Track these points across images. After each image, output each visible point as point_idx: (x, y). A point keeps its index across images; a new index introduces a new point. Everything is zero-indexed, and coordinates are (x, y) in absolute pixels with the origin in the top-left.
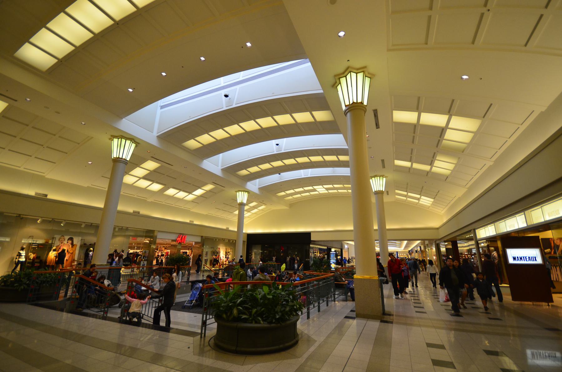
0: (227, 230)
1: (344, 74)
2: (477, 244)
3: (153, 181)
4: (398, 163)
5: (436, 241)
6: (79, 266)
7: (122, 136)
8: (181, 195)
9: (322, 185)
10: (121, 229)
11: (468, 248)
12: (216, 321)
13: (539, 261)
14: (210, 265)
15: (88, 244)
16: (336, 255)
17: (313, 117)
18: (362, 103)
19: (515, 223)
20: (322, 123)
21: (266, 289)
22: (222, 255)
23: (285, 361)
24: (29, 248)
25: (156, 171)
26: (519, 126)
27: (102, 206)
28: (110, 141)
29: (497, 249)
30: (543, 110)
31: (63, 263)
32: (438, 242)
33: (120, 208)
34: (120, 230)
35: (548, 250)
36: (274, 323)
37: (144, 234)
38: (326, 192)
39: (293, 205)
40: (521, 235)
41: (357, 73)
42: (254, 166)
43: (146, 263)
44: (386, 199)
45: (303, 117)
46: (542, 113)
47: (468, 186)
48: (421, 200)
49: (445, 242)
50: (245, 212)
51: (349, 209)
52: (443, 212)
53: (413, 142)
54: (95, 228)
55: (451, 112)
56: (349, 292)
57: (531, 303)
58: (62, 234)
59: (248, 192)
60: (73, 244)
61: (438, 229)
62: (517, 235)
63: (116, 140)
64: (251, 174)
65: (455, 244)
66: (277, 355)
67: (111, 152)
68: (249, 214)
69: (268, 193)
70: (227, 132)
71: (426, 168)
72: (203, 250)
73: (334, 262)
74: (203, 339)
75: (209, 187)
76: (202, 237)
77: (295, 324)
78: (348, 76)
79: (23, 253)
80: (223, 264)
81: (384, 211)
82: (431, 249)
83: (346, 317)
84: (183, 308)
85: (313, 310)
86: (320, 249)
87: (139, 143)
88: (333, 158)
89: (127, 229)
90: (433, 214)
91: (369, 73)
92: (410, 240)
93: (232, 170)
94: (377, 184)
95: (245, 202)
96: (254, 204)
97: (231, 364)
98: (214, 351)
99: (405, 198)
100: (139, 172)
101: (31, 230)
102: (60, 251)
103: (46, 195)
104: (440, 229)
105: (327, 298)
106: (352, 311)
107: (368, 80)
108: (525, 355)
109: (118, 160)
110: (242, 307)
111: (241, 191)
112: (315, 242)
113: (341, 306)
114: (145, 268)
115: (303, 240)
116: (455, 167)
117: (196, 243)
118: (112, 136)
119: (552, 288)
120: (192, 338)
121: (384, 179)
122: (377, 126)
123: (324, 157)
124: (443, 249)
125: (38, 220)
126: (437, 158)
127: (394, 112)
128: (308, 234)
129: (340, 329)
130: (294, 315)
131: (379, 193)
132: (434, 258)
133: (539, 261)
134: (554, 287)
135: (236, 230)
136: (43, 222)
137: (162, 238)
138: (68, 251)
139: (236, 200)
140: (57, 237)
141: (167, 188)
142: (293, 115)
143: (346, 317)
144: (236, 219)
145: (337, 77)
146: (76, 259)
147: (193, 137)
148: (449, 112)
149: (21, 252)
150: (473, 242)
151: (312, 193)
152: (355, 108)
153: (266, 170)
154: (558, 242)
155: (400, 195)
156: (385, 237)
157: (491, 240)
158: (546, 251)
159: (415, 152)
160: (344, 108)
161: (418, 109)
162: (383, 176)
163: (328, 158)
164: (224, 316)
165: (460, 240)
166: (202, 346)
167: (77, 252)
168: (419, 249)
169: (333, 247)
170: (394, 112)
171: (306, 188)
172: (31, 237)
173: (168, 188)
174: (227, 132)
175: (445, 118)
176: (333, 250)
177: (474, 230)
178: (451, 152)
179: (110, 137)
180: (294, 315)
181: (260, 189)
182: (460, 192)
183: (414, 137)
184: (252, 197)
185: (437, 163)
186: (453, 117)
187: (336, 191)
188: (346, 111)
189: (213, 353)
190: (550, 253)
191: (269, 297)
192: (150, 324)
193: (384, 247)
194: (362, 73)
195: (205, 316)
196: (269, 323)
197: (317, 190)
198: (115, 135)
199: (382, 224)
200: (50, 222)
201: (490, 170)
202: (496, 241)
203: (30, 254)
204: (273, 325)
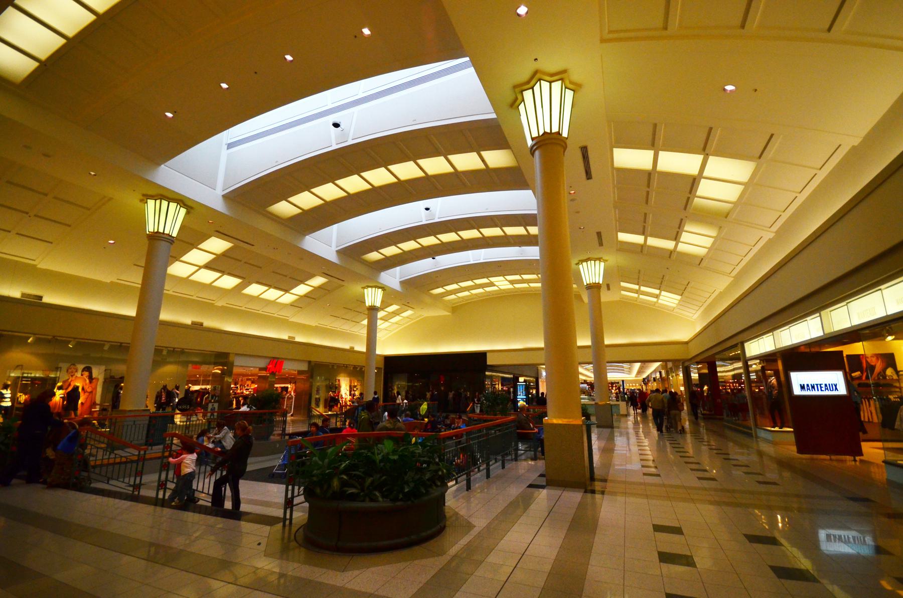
0: (351, 350)
1: (528, 84)
2: (746, 367)
3: (223, 272)
4: (623, 237)
5: (684, 361)
6: (104, 413)
7: (161, 195)
8: (272, 294)
9: (504, 276)
10: (173, 352)
11: (732, 373)
12: (306, 500)
13: (842, 390)
14: (325, 407)
15: (117, 377)
16: (527, 388)
17: (483, 161)
18: (558, 133)
19: (804, 331)
20: (498, 171)
21: (388, 446)
22: (344, 391)
23: (416, 562)
24: (17, 385)
25: (225, 255)
26: (815, 171)
27: (131, 312)
28: (141, 204)
29: (777, 374)
30: (856, 144)
31: (76, 409)
32: (686, 364)
33: (164, 316)
34: (161, 356)
35: (857, 374)
36: (401, 500)
37: (213, 360)
38: (511, 286)
39: (456, 308)
40: (813, 350)
41: (550, 82)
42: (390, 245)
43: (216, 405)
44: (606, 297)
45: (466, 161)
46: (854, 148)
47: (734, 274)
48: (661, 297)
49: (698, 363)
50: (379, 322)
51: (536, 313)
52: (696, 316)
53: (647, 203)
54: (122, 348)
55: (707, 151)
56: (537, 446)
57: (828, 457)
58: (73, 361)
59: (383, 288)
60: (91, 378)
61: (687, 343)
62: (808, 350)
63: (151, 202)
64: (387, 258)
65: (712, 367)
66: (405, 552)
67: (143, 223)
68: (387, 324)
69: (417, 289)
70: (341, 189)
71: (669, 244)
72: (311, 383)
73: (522, 399)
74: (287, 528)
75: (318, 281)
76: (310, 362)
77: (441, 499)
78: (537, 88)
79: (7, 393)
80: (346, 405)
81: (601, 316)
82: (677, 375)
83: (531, 486)
84: (268, 476)
85: (478, 476)
86: (503, 378)
87: (192, 208)
88: (519, 231)
89: (182, 352)
90: (680, 319)
91: (571, 82)
92: (645, 362)
93: (354, 252)
94: (592, 272)
95: (378, 304)
96: (394, 308)
97: (324, 570)
98: (303, 549)
99: (636, 295)
100: (196, 256)
101: (17, 355)
102: (70, 389)
103: (40, 298)
104: (690, 344)
105: (503, 456)
106: (541, 475)
107: (569, 94)
108: (816, 535)
109: (157, 237)
110: (347, 475)
111: (371, 287)
112: (493, 368)
113: (527, 467)
114: (216, 414)
115: (476, 362)
116: (714, 244)
117: (300, 372)
118: (144, 195)
119: (861, 434)
120: (268, 528)
121: (602, 264)
122: (589, 175)
123: (505, 229)
124: (695, 376)
125: (29, 338)
126: (686, 228)
127: (615, 150)
128: (482, 355)
129: (523, 503)
130: (437, 486)
131: (594, 288)
132: (682, 389)
133: (842, 390)
134: (865, 432)
135: (364, 349)
136: (38, 341)
137: (241, 365)
138: (83, 389)
139: (364, 302)
140: (64, 366)
141: (246, 283)
142: (450, 157)
143: (531, 486)
144: (364, 332)
145: (518, 90)
146: (98, 399)
147: (285, 197)
148: (704, 149)
149: (4, 391)
150: (740, 364)
151: (488, 289)
152: (549, 142)
153: (411, 252)
154: (873, 361)
155: (628, 290)
156: (600, 355)
157: (767, 359)
158: (853, 375)
159: (650, 218)
160: (530, 143)
161: (653, 144)
162: (600, 259)
163: (511, 231)
164: (318, 491)
165: (723, 360)
166: (286, 541)
167: (99, 389)
168: (658, 375)
169: (522, 376)
170: (615, 150)
171: (478, 282)
172: (19, 367)
173: (250, 284)
174: (341, 189)
175: (698, 159)
176: (521, 379)
177: (742, 343)
178: (707, 217)
179: (142, 198)
180: (437, 486)
181: (403, 283)
182: (721, 284)
183: (648, 193)
184: (390, 296)
185: (685, 237)
186: (711, 157)
187: (525, 285)
188: (532, 147)
189: (302, 553)
190: (860, 378)
191: (392, 457)
192: (206, 507)
193: (600, 372)
194: (560, 82)
195: (290, 487)
196: (393, 500)
197: (496, 283)
198: (150, 193)
199: (597, 337)
200: (49, 341)
201: (770, 246)
202: (775, 361)
203: (19, 394)
204: (399, 503)
